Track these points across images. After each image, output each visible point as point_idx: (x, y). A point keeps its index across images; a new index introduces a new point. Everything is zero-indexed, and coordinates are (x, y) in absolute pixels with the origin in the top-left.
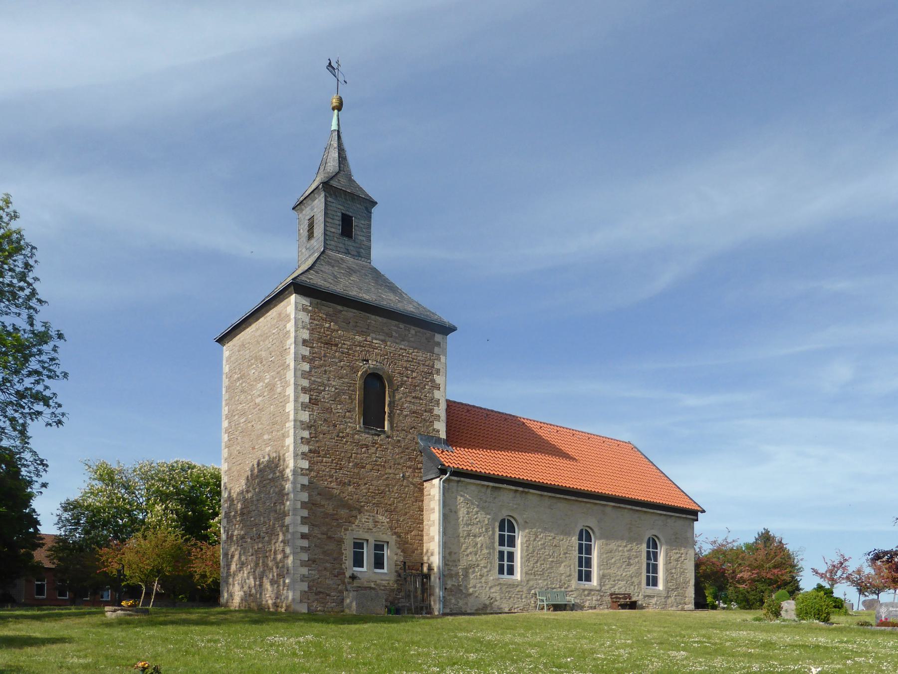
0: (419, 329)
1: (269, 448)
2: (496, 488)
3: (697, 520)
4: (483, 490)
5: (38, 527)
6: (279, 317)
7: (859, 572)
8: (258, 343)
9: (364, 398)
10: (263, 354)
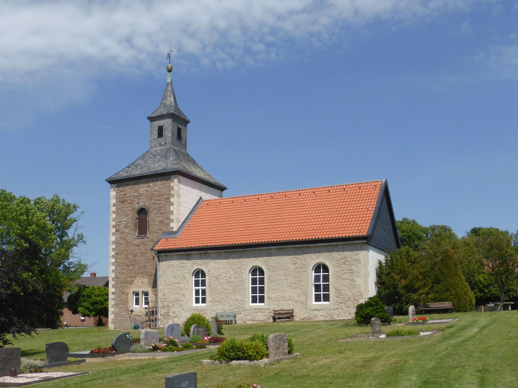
2: (188, 254)
9: (388, 195)
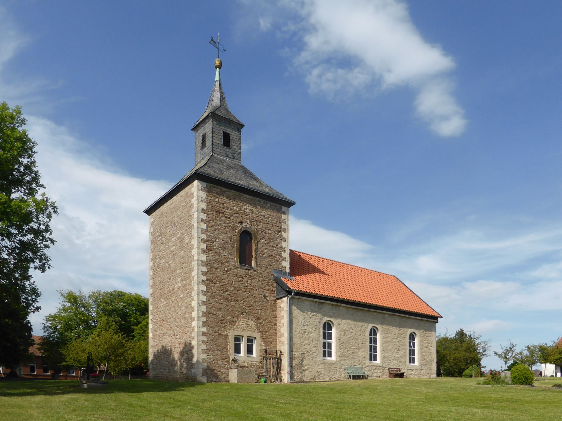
0: (273, 204)
1: (181, 278)
3: (437, 323)
4: (313, 304)
5: (31, 332)
6: (186, 195)
7: (521, 353)
8: (172, 212)
10: (176, 219)
